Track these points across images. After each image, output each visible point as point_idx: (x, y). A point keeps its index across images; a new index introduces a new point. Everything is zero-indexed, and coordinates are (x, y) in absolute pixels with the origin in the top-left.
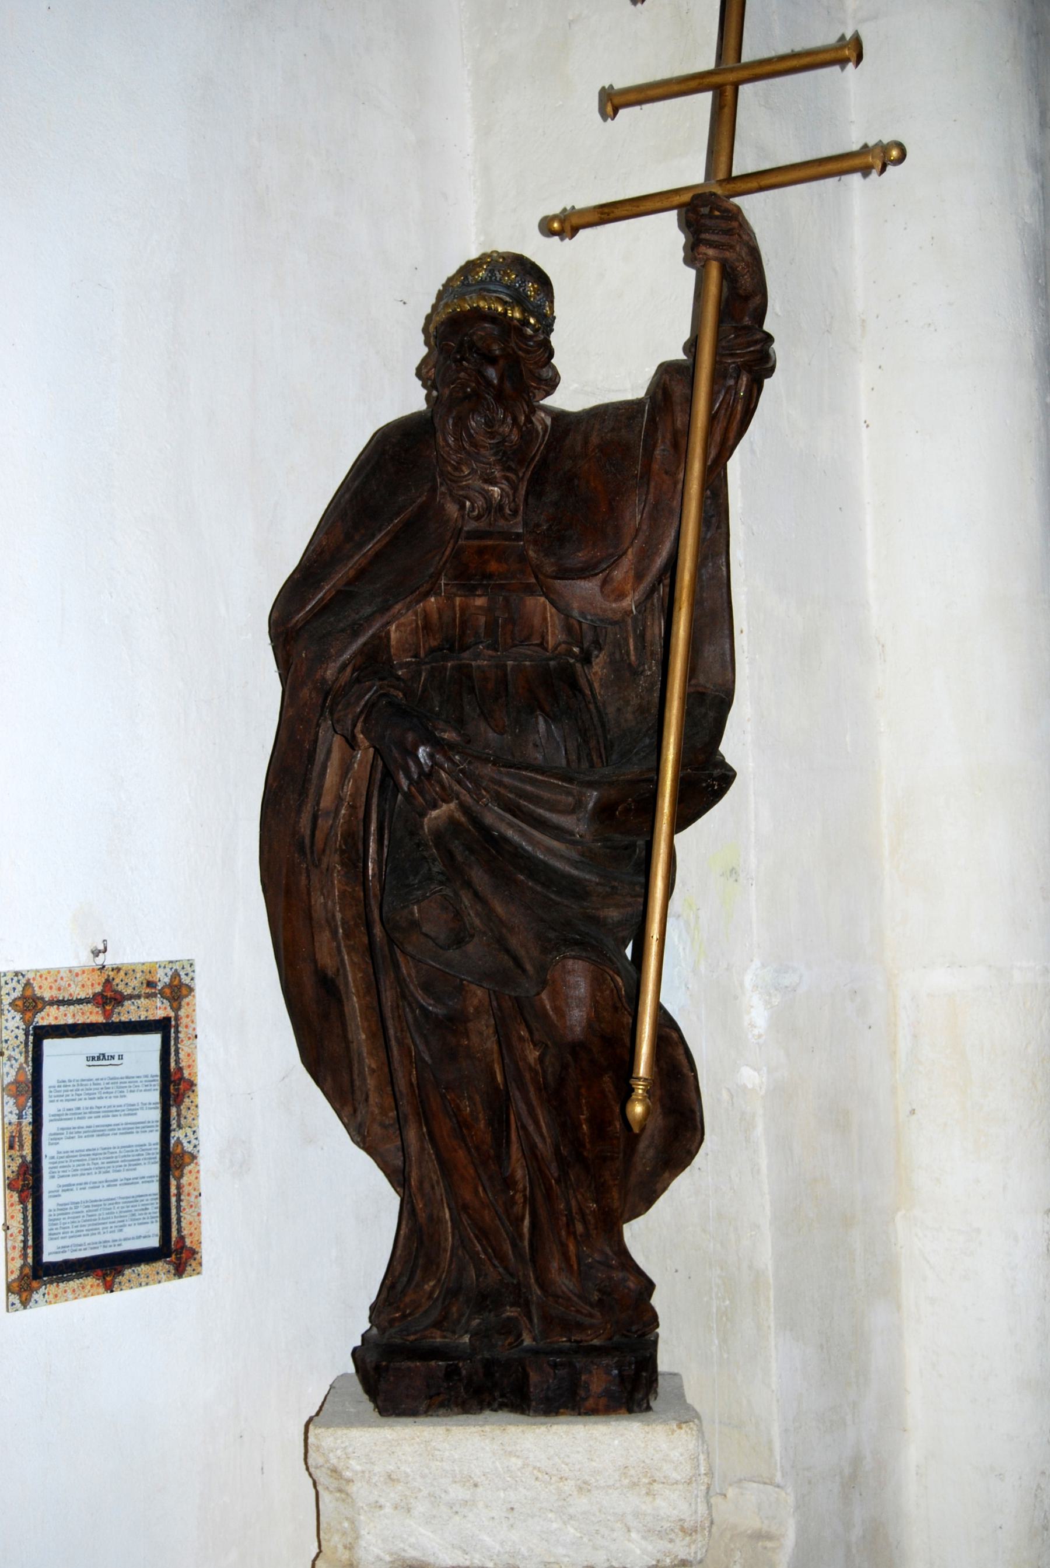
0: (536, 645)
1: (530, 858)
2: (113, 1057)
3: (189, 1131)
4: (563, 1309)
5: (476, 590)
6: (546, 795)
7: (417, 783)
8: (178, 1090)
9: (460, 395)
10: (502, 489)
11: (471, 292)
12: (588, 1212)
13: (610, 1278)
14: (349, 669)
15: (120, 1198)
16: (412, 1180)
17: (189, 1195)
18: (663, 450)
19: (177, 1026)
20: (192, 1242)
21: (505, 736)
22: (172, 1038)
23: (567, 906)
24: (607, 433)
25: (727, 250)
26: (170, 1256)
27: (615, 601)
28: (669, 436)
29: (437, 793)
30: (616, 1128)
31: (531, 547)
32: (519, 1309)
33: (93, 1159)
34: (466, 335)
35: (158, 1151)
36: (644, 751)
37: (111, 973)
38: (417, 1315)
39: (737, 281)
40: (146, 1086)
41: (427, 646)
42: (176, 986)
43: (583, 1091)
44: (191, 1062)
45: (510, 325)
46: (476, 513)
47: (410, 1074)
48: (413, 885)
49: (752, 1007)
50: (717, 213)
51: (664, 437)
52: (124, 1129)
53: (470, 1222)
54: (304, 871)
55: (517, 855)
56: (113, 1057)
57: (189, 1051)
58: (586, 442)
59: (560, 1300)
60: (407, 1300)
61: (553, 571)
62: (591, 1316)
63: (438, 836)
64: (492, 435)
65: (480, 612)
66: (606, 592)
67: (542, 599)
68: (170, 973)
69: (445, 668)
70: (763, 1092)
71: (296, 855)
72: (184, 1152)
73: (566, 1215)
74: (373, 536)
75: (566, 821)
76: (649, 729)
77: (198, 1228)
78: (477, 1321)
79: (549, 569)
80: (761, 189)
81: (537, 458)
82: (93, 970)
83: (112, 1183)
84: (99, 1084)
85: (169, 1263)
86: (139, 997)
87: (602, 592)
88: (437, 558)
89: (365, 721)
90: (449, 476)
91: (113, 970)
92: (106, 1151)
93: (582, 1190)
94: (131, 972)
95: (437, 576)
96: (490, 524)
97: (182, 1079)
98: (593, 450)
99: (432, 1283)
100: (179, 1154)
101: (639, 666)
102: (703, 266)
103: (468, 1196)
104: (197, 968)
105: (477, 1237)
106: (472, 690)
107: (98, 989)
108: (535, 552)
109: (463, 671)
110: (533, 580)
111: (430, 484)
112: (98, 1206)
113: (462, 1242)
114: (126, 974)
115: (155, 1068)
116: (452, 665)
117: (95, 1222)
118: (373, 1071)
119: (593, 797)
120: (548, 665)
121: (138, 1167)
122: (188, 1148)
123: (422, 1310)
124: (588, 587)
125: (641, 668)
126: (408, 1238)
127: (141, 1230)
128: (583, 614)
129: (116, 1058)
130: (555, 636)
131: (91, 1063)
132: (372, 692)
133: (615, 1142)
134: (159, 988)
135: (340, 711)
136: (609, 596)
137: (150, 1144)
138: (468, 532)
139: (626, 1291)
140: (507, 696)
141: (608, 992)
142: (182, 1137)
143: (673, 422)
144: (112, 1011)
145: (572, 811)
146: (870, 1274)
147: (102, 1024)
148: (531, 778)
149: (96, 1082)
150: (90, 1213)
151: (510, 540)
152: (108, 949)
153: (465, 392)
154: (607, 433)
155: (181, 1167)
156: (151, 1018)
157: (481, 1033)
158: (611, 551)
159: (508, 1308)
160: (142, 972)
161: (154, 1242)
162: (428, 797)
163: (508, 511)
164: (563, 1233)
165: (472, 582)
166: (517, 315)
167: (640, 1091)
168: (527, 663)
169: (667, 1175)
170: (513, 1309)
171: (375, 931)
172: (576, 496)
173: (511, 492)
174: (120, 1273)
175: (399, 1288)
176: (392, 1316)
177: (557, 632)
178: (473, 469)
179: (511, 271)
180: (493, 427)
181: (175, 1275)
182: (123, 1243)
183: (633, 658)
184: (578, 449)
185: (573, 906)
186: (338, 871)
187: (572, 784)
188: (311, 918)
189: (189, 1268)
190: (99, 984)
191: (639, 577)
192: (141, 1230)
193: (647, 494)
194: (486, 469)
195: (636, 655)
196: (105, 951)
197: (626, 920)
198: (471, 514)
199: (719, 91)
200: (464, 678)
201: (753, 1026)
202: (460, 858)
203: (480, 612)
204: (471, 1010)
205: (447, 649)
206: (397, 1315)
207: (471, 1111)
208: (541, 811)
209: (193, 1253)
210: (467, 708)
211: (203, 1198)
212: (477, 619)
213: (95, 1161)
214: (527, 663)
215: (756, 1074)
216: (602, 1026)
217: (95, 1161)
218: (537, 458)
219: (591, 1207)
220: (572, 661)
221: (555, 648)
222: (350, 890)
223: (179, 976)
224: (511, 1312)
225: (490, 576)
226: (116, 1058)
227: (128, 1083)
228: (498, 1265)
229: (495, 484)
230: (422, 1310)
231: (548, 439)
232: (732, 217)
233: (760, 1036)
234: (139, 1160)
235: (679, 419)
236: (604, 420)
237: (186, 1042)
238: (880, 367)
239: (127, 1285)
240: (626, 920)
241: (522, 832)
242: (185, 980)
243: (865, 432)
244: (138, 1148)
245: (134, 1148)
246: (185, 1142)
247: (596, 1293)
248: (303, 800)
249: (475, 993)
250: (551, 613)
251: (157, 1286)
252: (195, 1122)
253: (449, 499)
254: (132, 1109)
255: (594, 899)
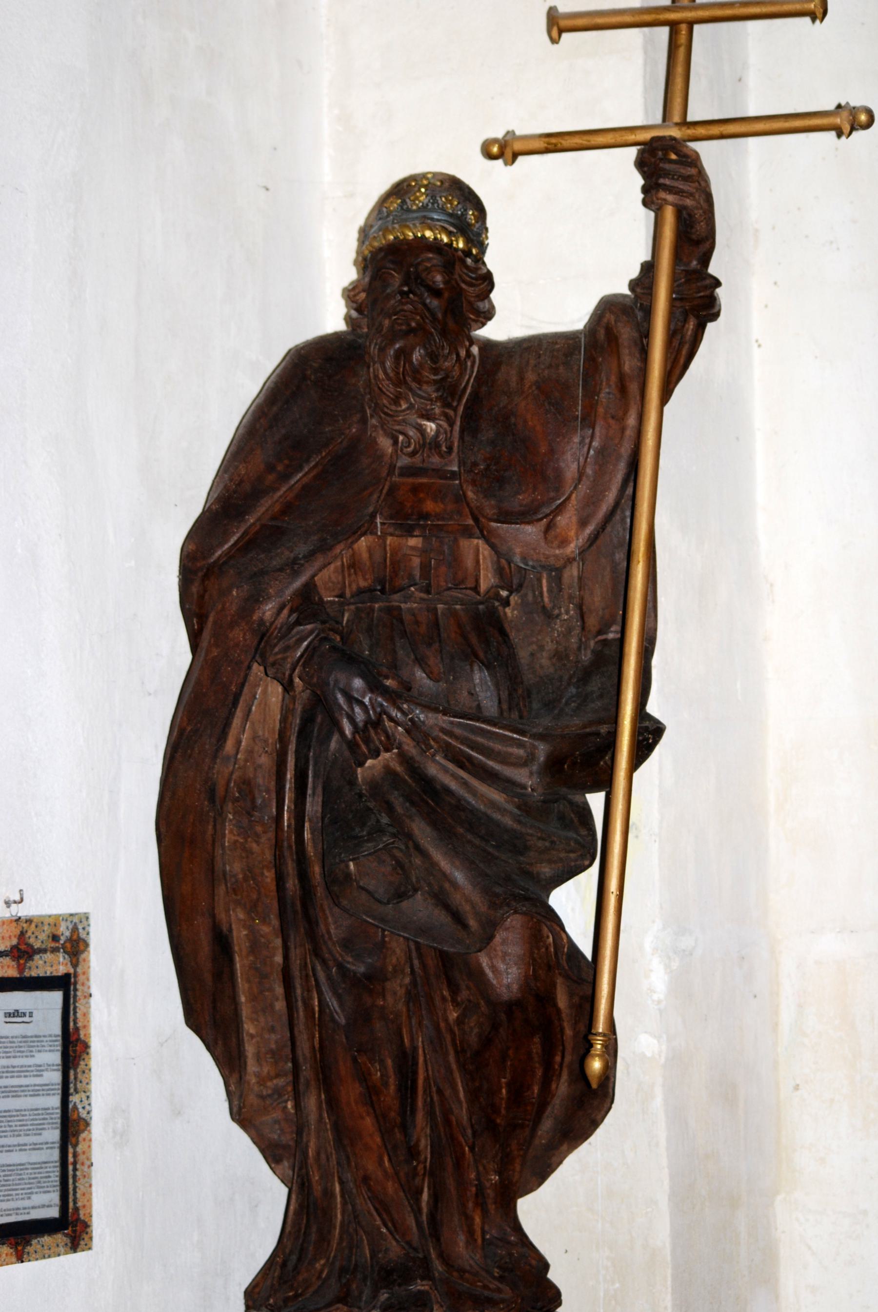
0: (471, 589)
1: (473, 811)
2: (24, 1014)
3: (83, 1095)
4: (468, 1285)
5: (413, 530)
6: (498, 747)
7: (363, 731)
8: (75, 1051)
9: (404, 327)
10: (439, 426)
11: (414, 219)
12: (488, 1185)
13: (510, 1255)
14: (286, 612)
15: (30, 1164)
16: (310, 1150)
17: (83, 1164)
18: (609, 393)
19: (75, 983)
20: (84, 1215)
21: (441, 683)
22: (72, 996)
23: (503, 861)
24: (543, 370)
25: (686, 197)
26: (67, 1229)
27: (559, 547)
28: (613, 379)
29: (381, 742)
30: (533, 1093)
31: (470, 488)
32: (431, 1283)
33: (9, 1121)
34: (411, 265)
35: (59, 1115)
36: (574, 702)
37: (25, 925)
38: (308, 1295)
39: (692, 227)
40: (51, 1046)
41: (354, 587)
42: (75, 941)
43: (511, 1052)
44: (86, 1023)
45: (454, 255)
46: (410, 449)
47: (313, 1037)
48: (363, 837)
49: (651, 971)
50: (673, 157)
51: (608, 380)
52: (33, 1091)
53: (369, 1194)
54: (212, 820)
55: (459, 806)
56: (24, 1014)
57: (85, 1011)
58: (521, 379)
59: (467, 1275)
60: (300, 1278)
61: (494, 514)
62: (499, 1291)
63: (374, 786)
64: (435, 371)
65: (414, 553)
66: (549, 538)
67: (481, 542)
68: (70, 927)
69: (372, 609)
70: (663, 1060)
71: (206, 803)
72: (80, 1118)
73: (476, 1185)
74: (301, 468)
75: (521, 775)
76: (571, 678)
77: (90, 1200)
78: (386, 1295)
79: (490, 512)
80: (722, 137)
81: (468, 391)
82: (11, 921)
83: (23, 1148)
84: (14, 1042)
85: (66, 1235)
86: (45, 951)
87: (546, 538)
88: (375, 496)
89: (304, 666)
90: (386, 410)
91: (26, 921)
92: (18, 1113)
93: (485, 1161)
94: (40, 924)
95: (373, 516)
96: (424, 461)
97: (78, 1039)
98: (530, 387)
99: (322, 1262)
100: (75, 1120)
101: (553, 608)
102: (658, 209)
103: (371, 1166)
104: (92, 921)
105: (377, 1210)
106: (404, 634)
107: (15, 941)
108: (474, 493)
109: (394, 613)
110: (470, 522)
111: (358, 416)
112: (13, 1170)
113: (356, 1217)
114: (36, 926)
115: (56, 1028)
116: (380, 607)
117: (9, 1188)
118: (252, 1036)
119: (542, 750)
120: (478, 609)
121: (43, 1132)
122: (83, 1114)
123: (311, 1290)
124: (531, 532)
125: (556, 612)
126: (297, 1213)
127: (39, 1199)
128: (524, 559)
129: (28, 1015)
130: (487, 580)
131: (8, 1020)
132: (314, 635)
133: (529, 1108)
134: (62, 942)
135: (276, 654)
136: (552, 543)
137: (53, 1109)
138: (401, 468)
139: (528, 1267)
140: (440, 641)
141: (543, 950)
142: (78, 1101)
143: (620, 366)
144: (25, 964)
145: (525, 763)
146: (752, 1260)
147: (16, 978)
148: (482, 729)
149: (11, 1040)
150: (6, 1178)
151: (446, 478)
152: (24, 898)
153: (409, 325)
154: (543, 370)
155: (77, 1134)
156: (55, 974)
157: (395, 993)
158: (552, 494)
159: (419, 1281)
160: (49, 924)
161: (54, 1213)
162: (372, 745)
163: (444, 449)
164: (470, 1205)
165: (409, 522)
166: (461, 245)
167: (599, 1047)
168: (458, 607)
169: (564, 1147)
170: (424, 1283)
171: (288, 885)
172: (513, 435)
173: (448, 429)
174: (28, 1243)
175: (290, 1266)
176: (286, 1295)
177: (490, 575)
178: (411, 404)
179: (453, 197)
180: (437, 363)
181: (71, 1248)
182: (32, 1211)
183: (546, 600)
184: (513, 384)
185: (510, 861)
186: (230, 820)
187: (525, 736)
188: (213, 871)
189: (82, 1242)
190: (15, 936)
191: (583, 523)
192: (39, 1199)
193: (592, 437)
194: (427, 405)
195: (550, 597)
196: (22, 900)
197: (558, 876)
198: (405, 450)
199: (674, 26)
200: (395, 621)
201: (652, 991)
202: (400, 810)
203: (414, 553)
204: (390, 969)
205: (379, 591)
206: (291, 1294)
207: (382, 1075)
208: (491, 763)
209: (86, 1226)
210: (401, 653)
211: (93, 1168)
212: (410, 560)
213: (10, 1124)
214: (458, 607)
215: (655, 1041)
216: (538, 985)
217: (10, 1124)
218: (468, 391)
219: (492, 1180)
220: (497, 604)
221: (488, 592)
222: (242, 841)
223: (77, 929)
224: (423, 1285)
225: (426, 516)
226: (28, 1015)
227: (31, 1043)
228: (400, 1240)
229: (429, 419)
230: (311, 1290)
231: (478, 371)
232: (691, 163)
233: (659, 1002)
234: (43, 1124)
235: (627, 363)
236: (540, 354)
237: (83, 1001)
238: (775, 283)
239: (34, 1256)
240: (558, 876)
241: (465, 784)
242: (83, 935)
243: (756, 352)
244: (43, 1112)
245: (40, 1112)
246: (80, 1106)
247: (496, 1270)
248: (221, 745)
249: (394, 951)
250: (483, 555)
251: (57, 1258)
252: (88, 1086)
253: (381, 432)
254: (39, 1070)
255: (532, 854)
